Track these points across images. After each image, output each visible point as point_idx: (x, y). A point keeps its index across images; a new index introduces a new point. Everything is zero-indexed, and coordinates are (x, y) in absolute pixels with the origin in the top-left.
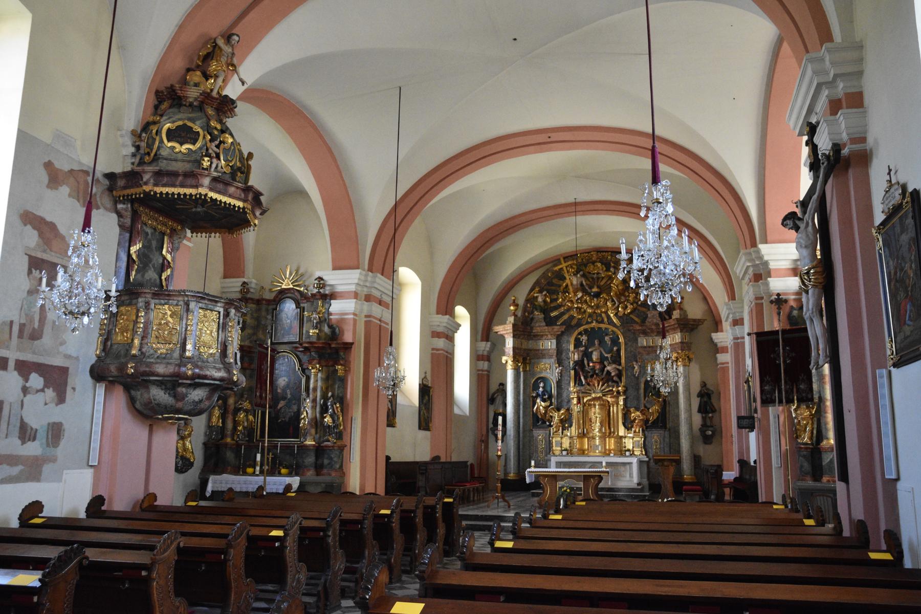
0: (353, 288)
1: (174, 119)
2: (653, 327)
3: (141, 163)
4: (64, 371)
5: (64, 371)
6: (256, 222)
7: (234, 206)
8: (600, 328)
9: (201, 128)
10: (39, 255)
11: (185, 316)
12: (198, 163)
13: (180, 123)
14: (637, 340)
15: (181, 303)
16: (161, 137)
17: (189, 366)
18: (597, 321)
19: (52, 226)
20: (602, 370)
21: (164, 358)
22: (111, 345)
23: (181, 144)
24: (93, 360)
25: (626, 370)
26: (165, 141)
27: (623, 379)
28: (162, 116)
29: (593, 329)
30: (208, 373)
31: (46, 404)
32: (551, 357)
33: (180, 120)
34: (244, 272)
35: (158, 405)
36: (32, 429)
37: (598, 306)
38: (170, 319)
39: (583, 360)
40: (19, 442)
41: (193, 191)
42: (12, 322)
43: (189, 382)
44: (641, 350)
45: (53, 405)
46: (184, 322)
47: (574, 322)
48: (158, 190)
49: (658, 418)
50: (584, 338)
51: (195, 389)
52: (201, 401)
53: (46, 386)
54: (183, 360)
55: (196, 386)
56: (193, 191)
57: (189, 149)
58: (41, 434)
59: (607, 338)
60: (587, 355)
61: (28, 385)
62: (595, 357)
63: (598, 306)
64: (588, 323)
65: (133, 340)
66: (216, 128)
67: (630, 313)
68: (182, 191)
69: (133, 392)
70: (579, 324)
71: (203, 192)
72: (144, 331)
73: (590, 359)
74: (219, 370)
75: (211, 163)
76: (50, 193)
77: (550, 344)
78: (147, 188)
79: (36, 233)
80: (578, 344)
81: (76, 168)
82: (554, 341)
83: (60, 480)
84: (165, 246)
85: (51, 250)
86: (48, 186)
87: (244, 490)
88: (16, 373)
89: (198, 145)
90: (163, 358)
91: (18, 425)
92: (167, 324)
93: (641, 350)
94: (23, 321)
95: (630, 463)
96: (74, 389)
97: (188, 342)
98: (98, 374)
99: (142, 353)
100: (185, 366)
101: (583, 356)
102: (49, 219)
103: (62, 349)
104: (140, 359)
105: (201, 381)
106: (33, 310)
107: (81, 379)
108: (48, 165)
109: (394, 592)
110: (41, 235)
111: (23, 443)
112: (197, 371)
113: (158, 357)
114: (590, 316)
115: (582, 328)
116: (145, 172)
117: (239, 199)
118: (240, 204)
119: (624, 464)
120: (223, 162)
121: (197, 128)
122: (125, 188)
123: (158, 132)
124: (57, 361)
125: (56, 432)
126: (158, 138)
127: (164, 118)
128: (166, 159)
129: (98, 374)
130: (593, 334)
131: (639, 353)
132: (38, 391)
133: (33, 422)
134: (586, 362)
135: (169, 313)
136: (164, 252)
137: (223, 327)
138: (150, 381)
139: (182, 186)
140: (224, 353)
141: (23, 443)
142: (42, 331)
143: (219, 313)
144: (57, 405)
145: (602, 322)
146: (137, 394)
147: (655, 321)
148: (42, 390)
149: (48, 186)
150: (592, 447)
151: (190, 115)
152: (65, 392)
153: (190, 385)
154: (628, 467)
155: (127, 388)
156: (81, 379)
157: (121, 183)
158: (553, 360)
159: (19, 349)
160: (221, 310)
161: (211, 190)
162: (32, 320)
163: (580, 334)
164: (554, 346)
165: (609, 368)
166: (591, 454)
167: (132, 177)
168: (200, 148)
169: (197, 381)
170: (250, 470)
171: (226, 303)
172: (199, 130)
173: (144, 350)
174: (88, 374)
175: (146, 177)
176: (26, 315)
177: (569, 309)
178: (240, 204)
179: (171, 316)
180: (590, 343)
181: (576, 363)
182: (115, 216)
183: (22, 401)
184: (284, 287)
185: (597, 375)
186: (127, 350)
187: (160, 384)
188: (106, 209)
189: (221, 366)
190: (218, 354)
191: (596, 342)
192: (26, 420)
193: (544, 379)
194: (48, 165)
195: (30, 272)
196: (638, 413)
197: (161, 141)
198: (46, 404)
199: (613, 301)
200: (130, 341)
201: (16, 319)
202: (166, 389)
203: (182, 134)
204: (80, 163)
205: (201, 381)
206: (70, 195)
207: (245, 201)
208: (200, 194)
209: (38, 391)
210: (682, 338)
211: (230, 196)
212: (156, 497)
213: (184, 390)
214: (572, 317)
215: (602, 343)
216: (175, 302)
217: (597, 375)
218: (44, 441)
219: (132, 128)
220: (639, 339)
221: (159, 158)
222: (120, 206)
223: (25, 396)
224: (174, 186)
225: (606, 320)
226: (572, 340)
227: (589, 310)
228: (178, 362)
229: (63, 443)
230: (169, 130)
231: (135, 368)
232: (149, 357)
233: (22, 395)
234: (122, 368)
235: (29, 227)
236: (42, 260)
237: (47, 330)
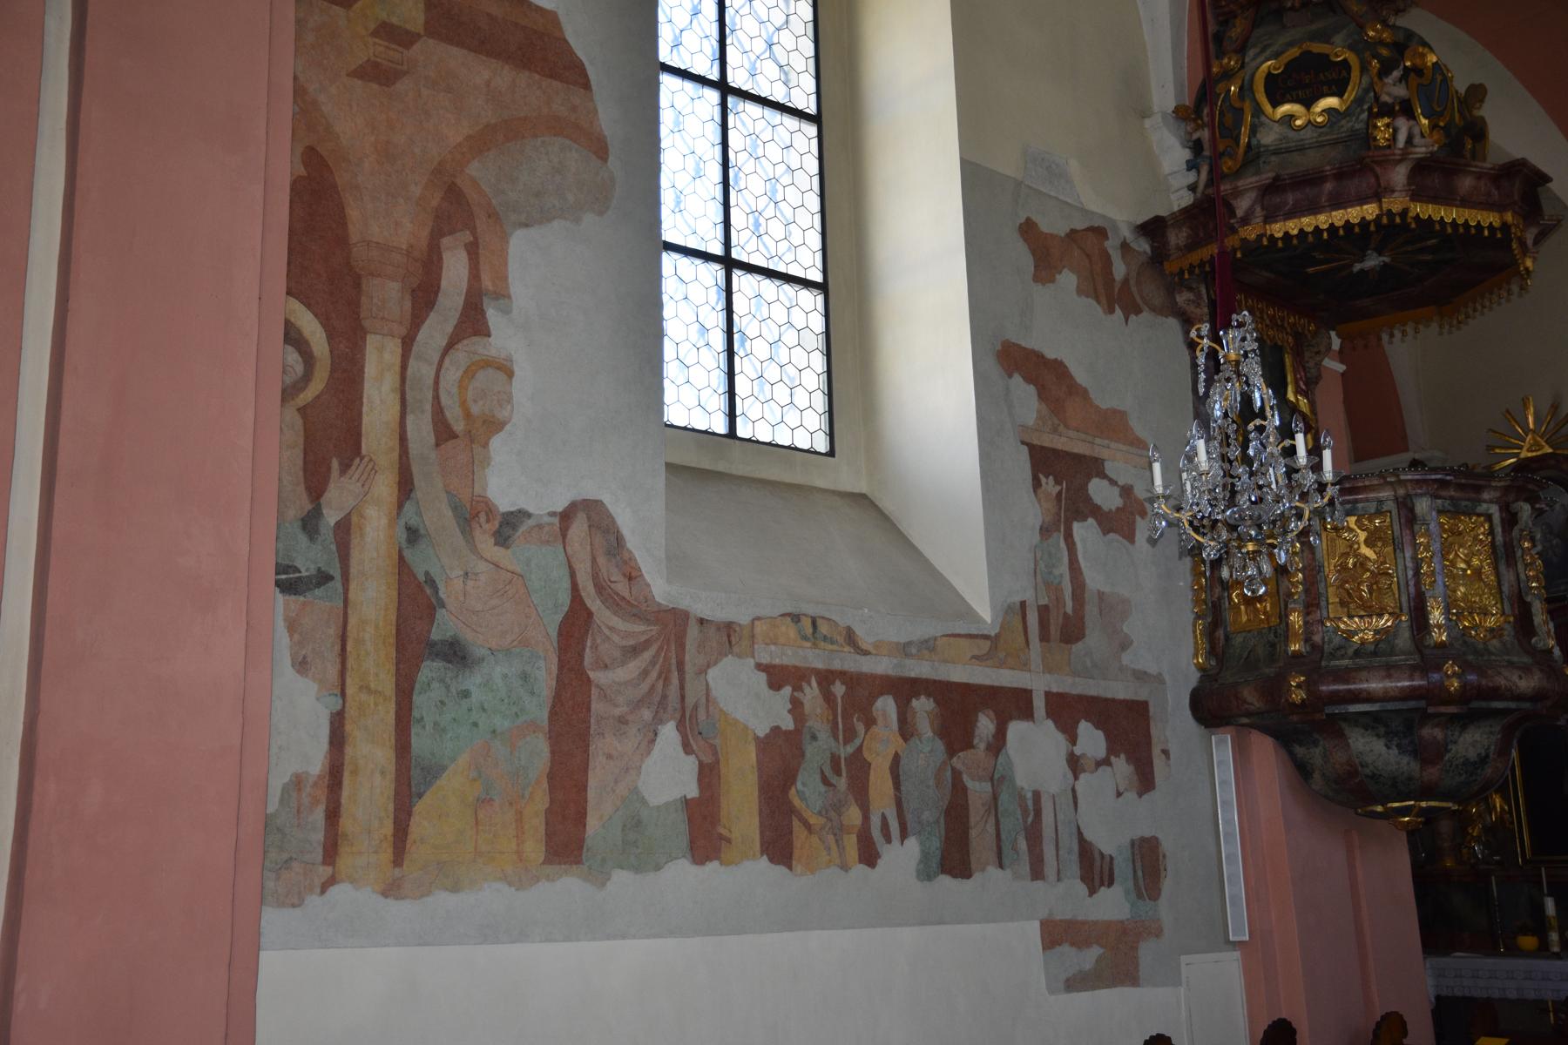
0: (729, 79)
1: (1274, 48)
3: (1215, 177)
4: (1138, 712)
5: (1138, 712)
6: (1529, 263)
7: (1479, 226)
9: (1351, 48)
10: (1048, 440)
11: (1407, 539)
12: (1367, 139)
13: (1294, 52)
15: (1390, 505)
16: (1255, 100)
17: (1450, 668)
19: (1058, 369)
21: (1375, 654)
22: (1227, 638)
23: (1308, 104)
24: (1194, 678)
26: (1268, 108)
28: (1241, 50)
30: (1501, 681)
31: (1119, 794)
33: (1291, 44)
34: (1404, 437)
35: (1374, 777)
36: (1102, 854)
38: (1366, 551)
40: (1082, 889)
41: (1370, 211)
42: (1023, 604)
43: (1452, 709)
45: (1131, 796)
46: (1408, 554)
48: (1277, 229)
51: (1464, 728)
52: (1483, 760)
53: (1112, 750)
54: (1428, 658)
55: (1465, 720)
56: (1370, 211)
57: (1329, 111)
58: (1122, 868)
61: (1078, 750)
65: (1283, 617)
66: (1382, 43)
68: (1338, 217)
69: (1300, 751)
71: (1396, 208)
72: (1306, 591)
74: (1526, 670)
75: (1395, 130)
76: (1042, 294)
78: (1250, 233)
79: (1032, 389)
81: (1080, 226)
83: (1177, 982)
84: (1289, 378)
85: (1067, 426)
86: (1037, 279)
87: (1531, 995)
88: (1050, 724)
89: (1351, 94)
90: (1378, 654)
91: (1076, 847)
92: (1362, 562)
94: (1044, 601)
96: (1165, 752)
97: (1430, 603)
98: (1210, 708)
99: (1314, 647)
100: (1439, 668)
102: (1050, 354)
103: (1126, 658)
104: (1314, 662)
105: (1484, 704)
106: (1056, 572)
107: (1175, 724)
108: (1028, 230)
110: (1043, 394)
111: (1092, 892)
112: (1472, 677)
113: (1357, 653)
116: (1237, 193)
117: (1488, 206)
118: (1490, 218)
120: (1425, 121)
121: (1340, 52)
122: (1192, 246)
123: (1246, 90)
124: (1119, 690)
125: (1148, 859)
126: (1248, 107)
127: (1251, 53)
128: (1276, 152)
129: (1210, 708)
132: (1099, 764)
133: (1109, 840)
135: (1362, 536)
136: (1291, 396)
137: (1504, 554)
138: (1346, 717)
139: (1338, 203)
140: (1524, 623)
141: (1092, 892)
142: (1082, 618)
143: (1489, 518)
144: (1140, 795)
146: (1314, 755)
148: (1106, 762)
149: (1037, 279)
151: (1314, 27)
152: (1150, 763)
153: (1453, 718)
155: (1286, 738)
156: (1175, 724)
157: (1177, 238)
159: (1048, 669)
160: (1494, 510)
161: (1415, 197)
162: (1059, 600)
167: (1207, 212)
168: (1359, 101)
169: (1475, 704)
170: (1528, 942)
171: (1506, 490)
172: (1348, 55)
173: (1317, 638)
174: (1188, 713)
175: (1242, 205)
176: (1047, 585)
178: (1490, 218)
179: (1368, 543)
182: (1173, 323)
183: (1074, 790)
184: (1524, 454)
186: (1273, 645)
187: (1372, 722)
188: (1153, 309)
189: (1526, 659)
190: (1509, 631)
192: (1088, 836)
194: (1028, 230)
195: (1037, 484)
197: (1258, 111)
198: (1119, 794)
200: (1274, 621)
201: (1029, 596)
202: (1389, 736)
203: (1301, 81)
204: (1085, 212)
205: (1484, 704)
206: (1080, 292)
207: (1499, 207)
208: (1390, 213)
209: (1099, 764)
211: (1465, 203)
212: (1404, 1024)
213: (1438, 733)
216: (1372, 507)
218: (1131, 884)
219: (1171, 105)
221: (1258, 156)
222: (1182, 298)
223: (1076, 778)
224: (1314, 209)
228: (1415, 659)
229: (1167, 885)
230: (1269, 77)
231: (1307, 686)
232: (1333, 656)
233: (1070, 775)
234: (1273, 689)
235: (1017, 379)
236: (1055, 451)
237: (1091, 611)
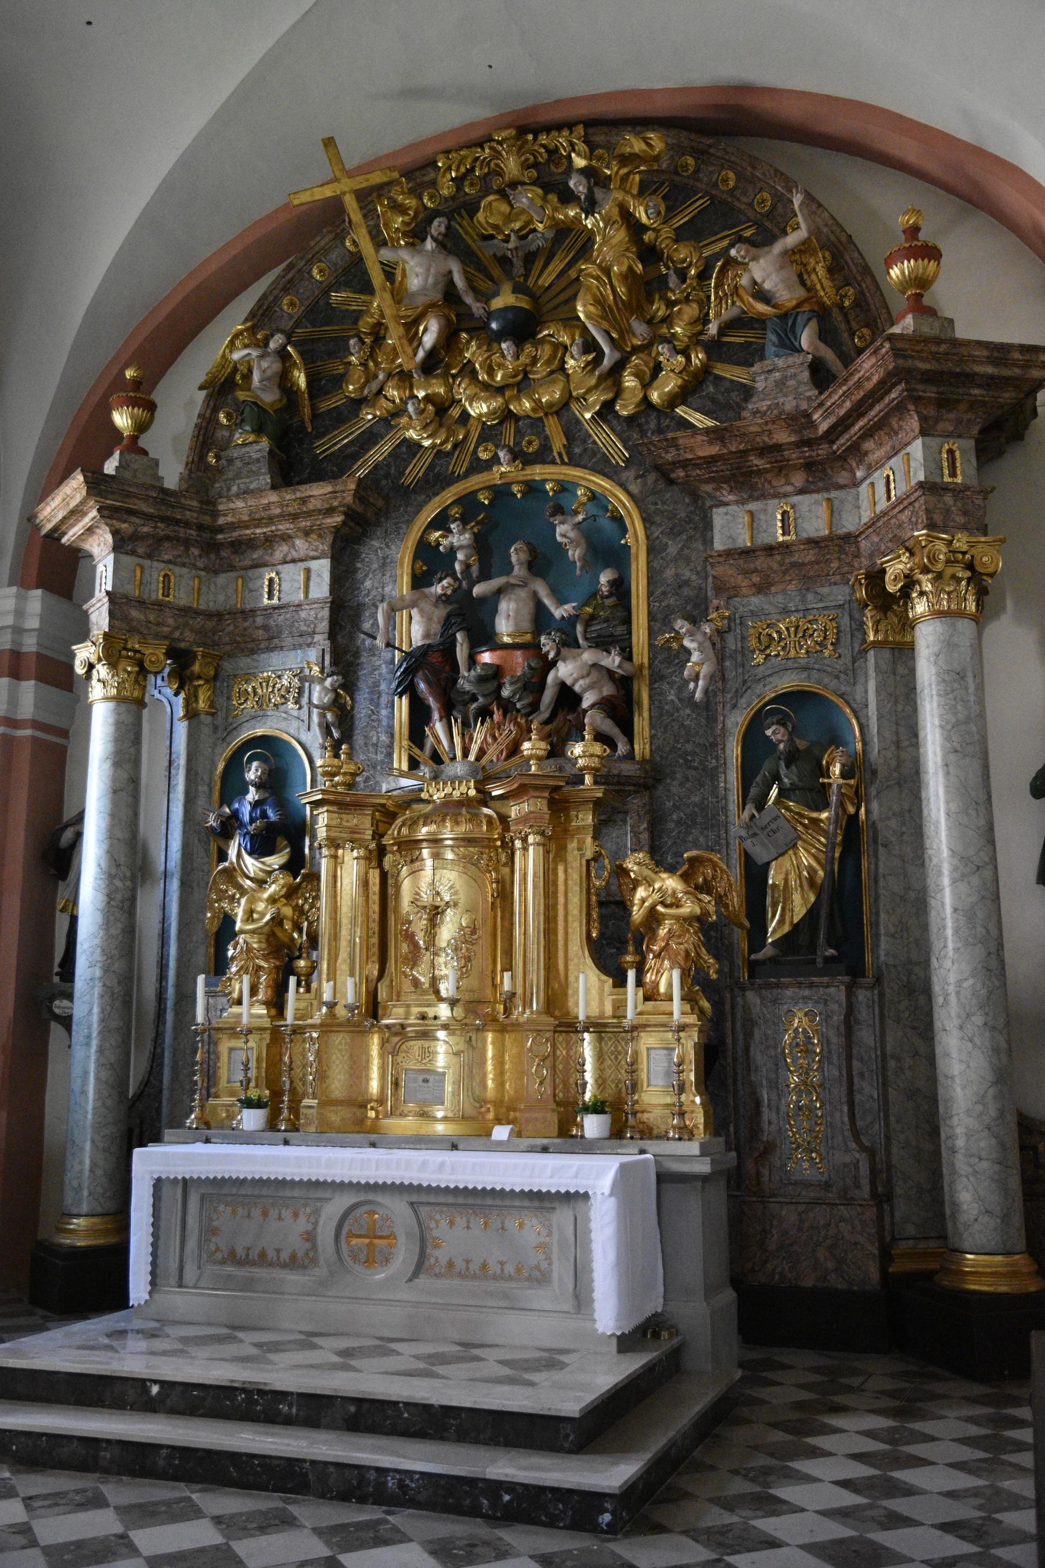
2: (783, 437)
8: (533, 488)
14: (707, 526)
18: (517, 455)
20: (534, 684)
25: (656, 678)
27: (641, 723)
29: (500, 493)
32: (304, 640)
37: (522, 383)
39: (448, 649)
44: (725, 570)
47: (415, 470)
49: (812, 913)
50: (458, 538)
59: (563, 531)
60: (471, 618)
62: (506, 625)
63: (522, 383)
64: (478, 466)
67: (682, 396)
70: (436, 480)
73: (483, 636)
77: (298, 581)
80: (430, 563)
82: (322, 568)
93: (725, 570)
95: (575, 1199)
101: (447, 624)
109: (989, 1432)
114: (488, 434)
115: (449, 496)
119: (541, 1200)
130: (496, 522)
131: (720, 588)
134: (461, 653)
145: (543, 456)
147: (789, 404)
150: (408, 1088)
154: (563, 1216)
158: (313, 655)
163: (441, 522)
164: (321, 588)
165: (565, 671)
166: (406, 1125)
177: (388, 422)
180: (488, 556)
181: (417, 661)
185: (507, 707)
191: (517, 555)
193: (269, 748)
196: (671, 883)
199: (590, 346)
210: (931, 461)
214: (414, 447)
215: (544, 561)
217: (507, 707)
220: (719, 517)
225: (558, 443)
226: (403, 554)
227: (479, 409)
